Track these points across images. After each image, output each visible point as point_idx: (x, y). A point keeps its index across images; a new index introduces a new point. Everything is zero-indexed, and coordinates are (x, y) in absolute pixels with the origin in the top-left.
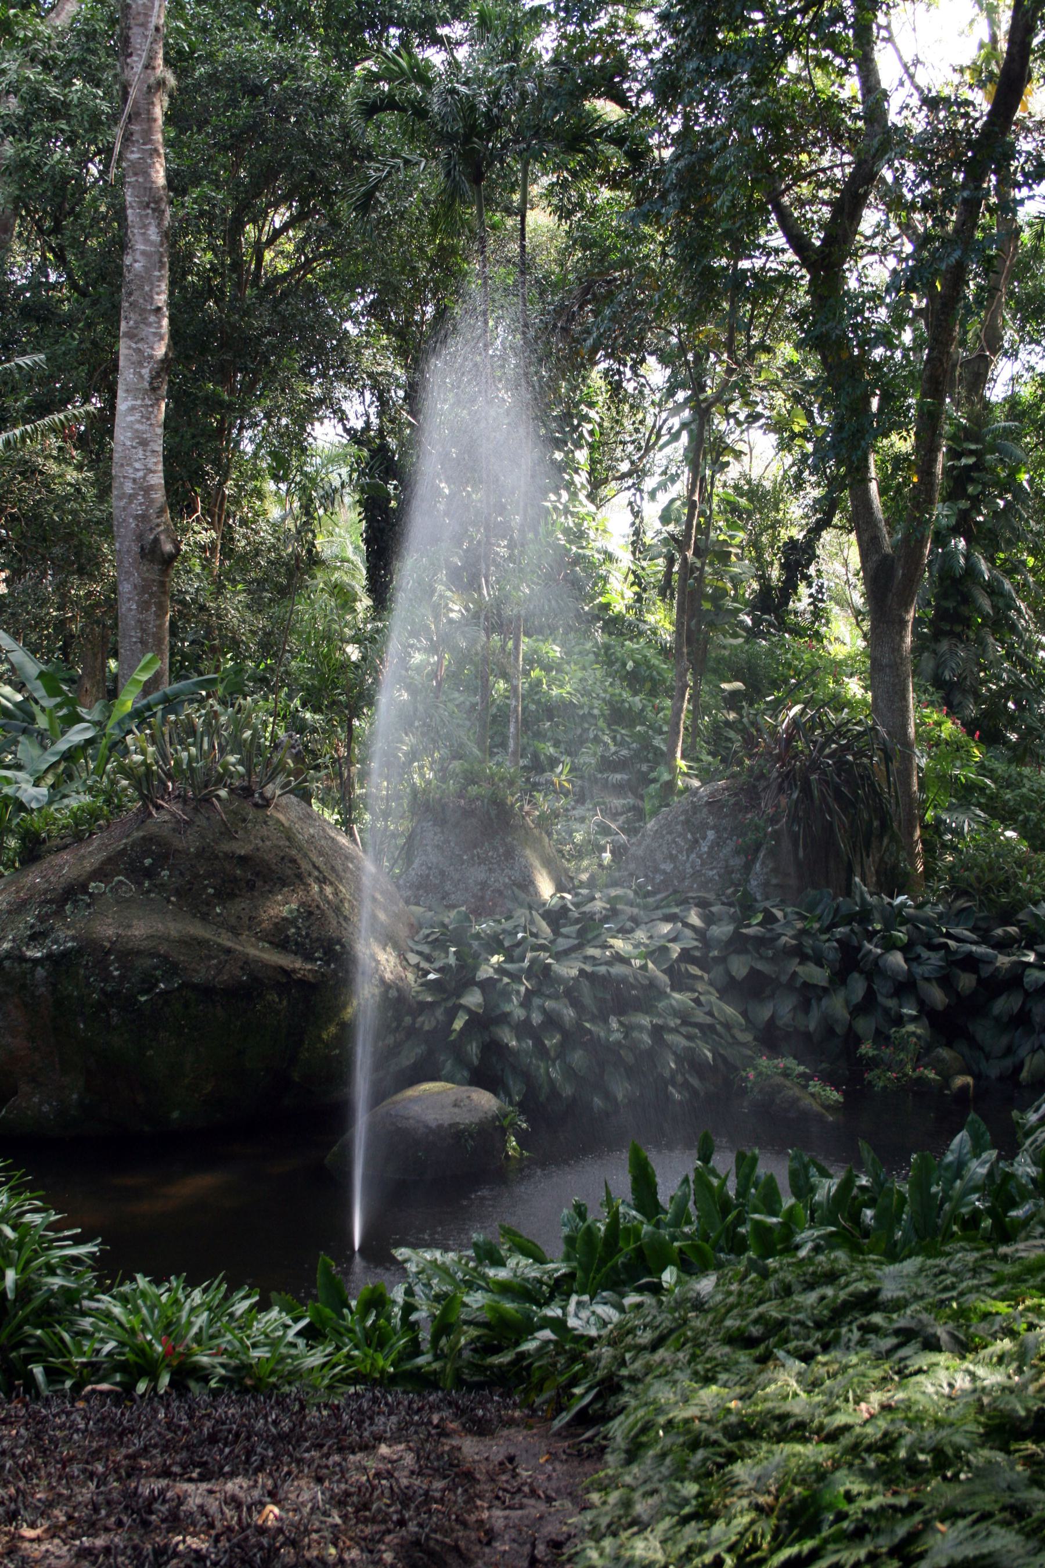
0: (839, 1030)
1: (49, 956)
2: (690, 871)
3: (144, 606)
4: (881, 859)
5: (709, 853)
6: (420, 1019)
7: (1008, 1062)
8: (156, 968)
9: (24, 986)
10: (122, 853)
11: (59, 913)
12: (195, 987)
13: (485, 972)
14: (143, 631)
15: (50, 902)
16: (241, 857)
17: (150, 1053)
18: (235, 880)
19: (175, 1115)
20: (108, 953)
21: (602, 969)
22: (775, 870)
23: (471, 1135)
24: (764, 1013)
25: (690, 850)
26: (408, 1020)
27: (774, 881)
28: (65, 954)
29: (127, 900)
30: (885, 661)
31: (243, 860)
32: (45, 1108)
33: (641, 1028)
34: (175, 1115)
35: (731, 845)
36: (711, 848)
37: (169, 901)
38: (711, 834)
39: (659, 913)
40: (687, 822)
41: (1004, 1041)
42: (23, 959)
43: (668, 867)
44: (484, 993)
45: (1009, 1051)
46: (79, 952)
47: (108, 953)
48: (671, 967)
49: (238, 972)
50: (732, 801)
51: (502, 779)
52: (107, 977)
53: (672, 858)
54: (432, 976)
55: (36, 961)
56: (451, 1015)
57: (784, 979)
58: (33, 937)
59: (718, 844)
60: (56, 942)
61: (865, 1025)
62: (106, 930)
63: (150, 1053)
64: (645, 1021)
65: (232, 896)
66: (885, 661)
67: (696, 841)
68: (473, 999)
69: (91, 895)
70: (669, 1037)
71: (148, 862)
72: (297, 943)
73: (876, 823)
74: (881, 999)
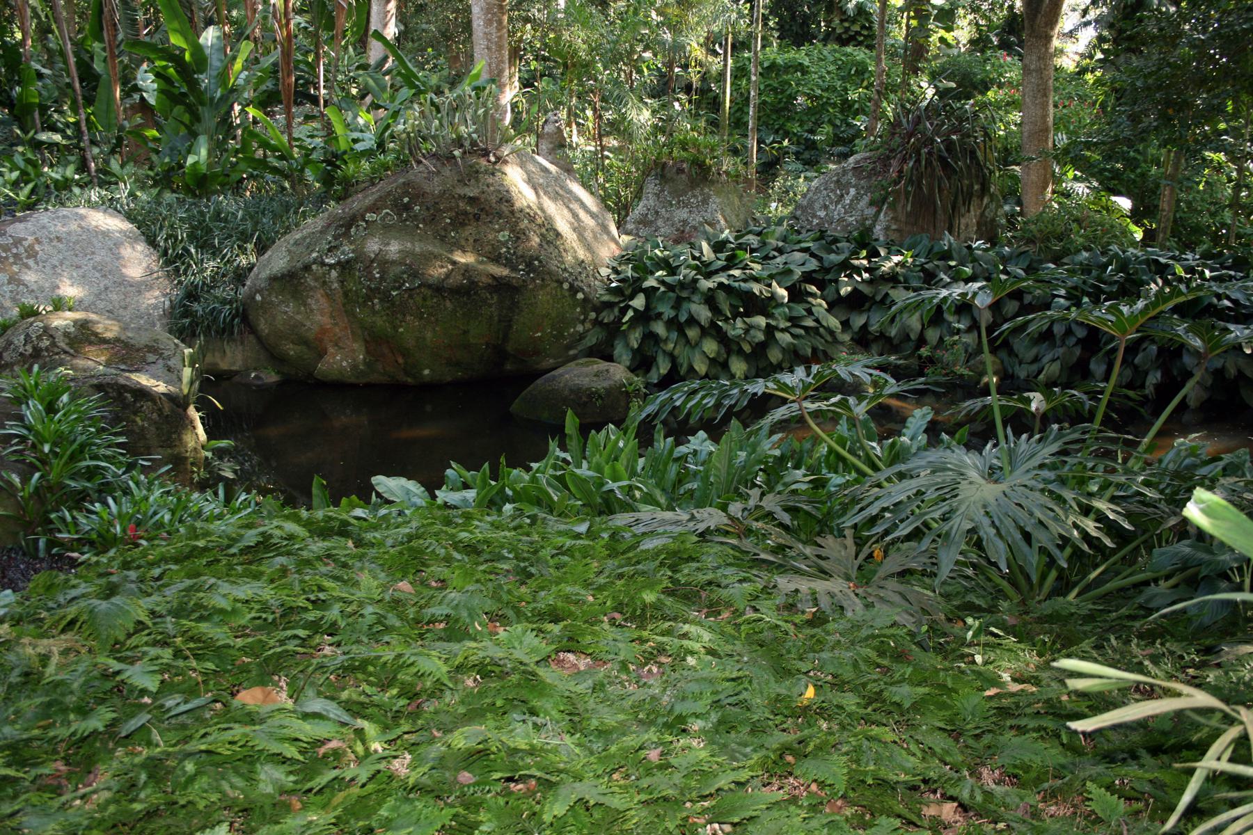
0: (912, 336)
1: (339, 263)
2: (836, 217)
3: (488, 23)
4: (982, 214)
5: (850, 205)
6: (604, 314)
7: (1035, 367)
8: (404, 272)
9: (324, 282)
10: (389, 193)
11: (347, 234)
12: (430, 286)
13: (651, 282)
14: (489, 40)
15: (342, 226)
16: (470, 198)
17: (401, 330)
18: (465, 213)
19: (426, 372)
20: (372, 261)
21: (736, 284)
22: (895, 219)
23: (600, 396)
24: (858, 321)
25: (837, 203)
26: (593, 315)
27: (894, 227)
28: (348, 262)
29: (391, 226)
30: (1033, 67)
31: (472, 200)
32: (344, 364)
33: (757, 328)
34: (426, 372)
35: (866, 199)
36: (852, 201)
37: (418, 227)
38: (853, 191)
39: (797, 247)
40: (838, 181)
41: (1034, 351)
42: (323, 264)
43: (822, 214)
44: (647, 298)
45: (1036, 359)
46: (356, 260)
47: (372, 261)
48: (794, 285)
49: (460, 277)
50: (871, 166)
51: (706, 147)
52: (372, 279)
53: (826, 207)
54: (614, 285)
55: (331, 266)
56: (623, 312)
57: (878, 298)
58: (330, 250)
59: (857, 198)
60: (343, 253)
61: (932, 335)
62: (373, 246)
63: (401, 330)
64: (761, 321)
65: (463, 225)
66: (1033, 67)
67: (842, 196)
68: (639, 302)
69: (367, 222)
70: (778, 335)
71: (406, 200)
72: (506, 259)
73: (976, 187)
74: (946, 316)
